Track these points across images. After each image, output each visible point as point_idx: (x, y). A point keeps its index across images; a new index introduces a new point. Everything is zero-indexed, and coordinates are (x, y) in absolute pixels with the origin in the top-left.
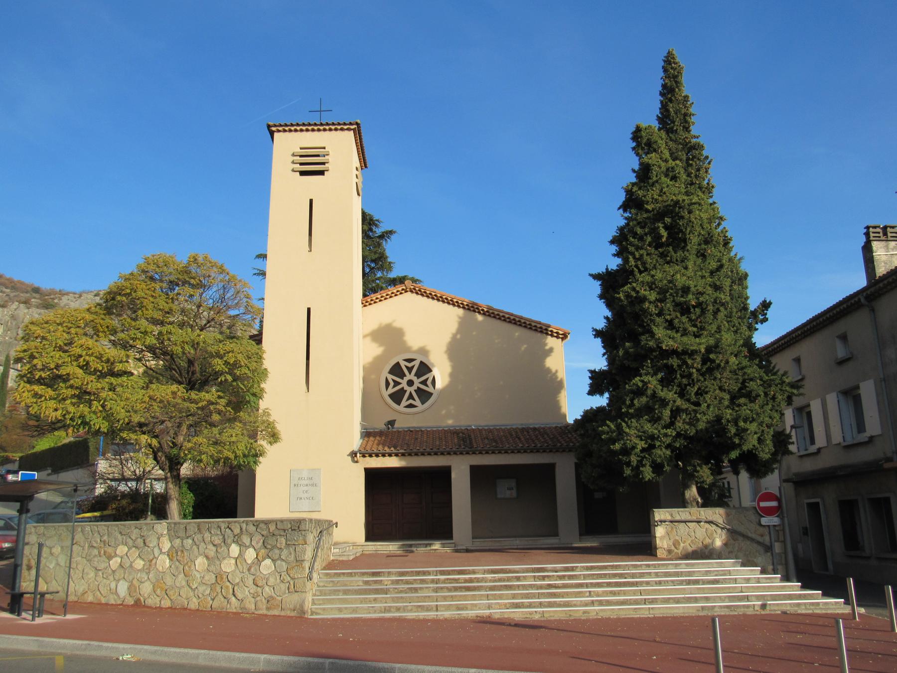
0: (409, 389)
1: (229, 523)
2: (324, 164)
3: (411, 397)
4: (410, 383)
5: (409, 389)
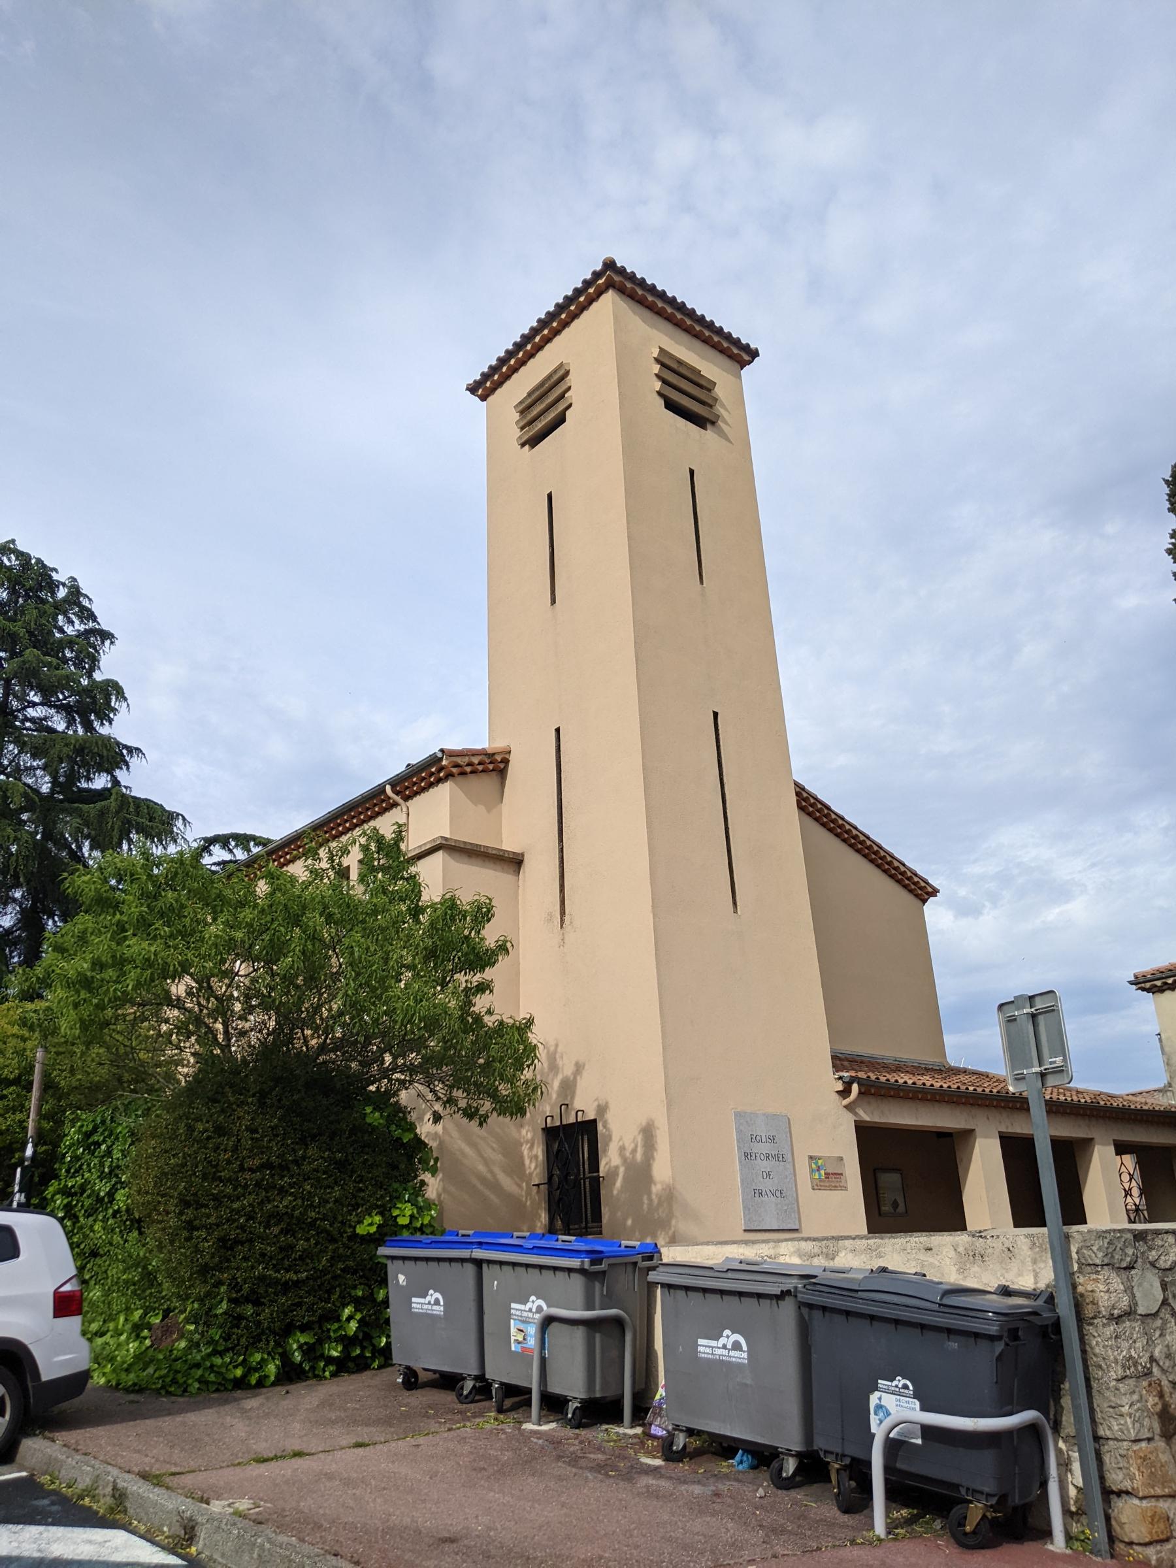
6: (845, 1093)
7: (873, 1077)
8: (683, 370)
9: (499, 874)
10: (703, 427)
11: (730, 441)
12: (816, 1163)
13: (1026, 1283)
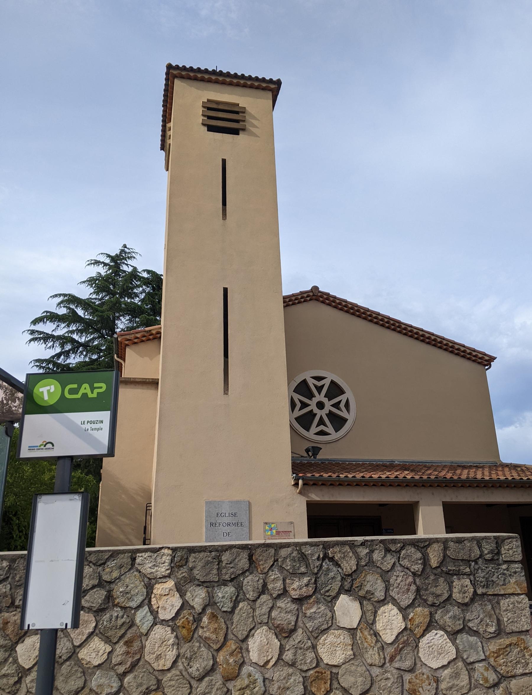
0: (319, 413)
1: (326, 546)
2: (237, 121)
3: (321, 422)
4: (320, 405)
5: (319, 413)
6: (296, 485)
7: (384, 477)
8: (221, 107)
9: (145, 391)
10: (238, 134)
11: (259, 137)
12: (270, 526)
13: (203, 595)
